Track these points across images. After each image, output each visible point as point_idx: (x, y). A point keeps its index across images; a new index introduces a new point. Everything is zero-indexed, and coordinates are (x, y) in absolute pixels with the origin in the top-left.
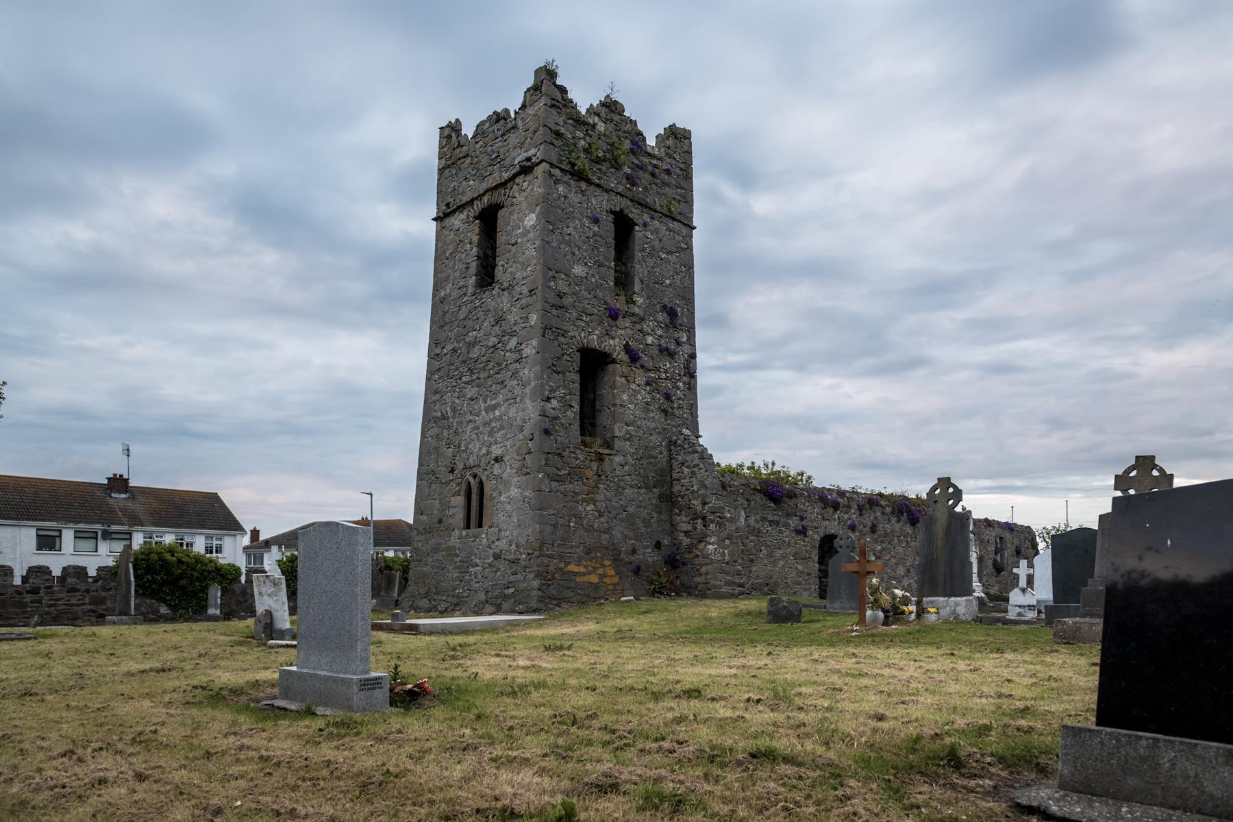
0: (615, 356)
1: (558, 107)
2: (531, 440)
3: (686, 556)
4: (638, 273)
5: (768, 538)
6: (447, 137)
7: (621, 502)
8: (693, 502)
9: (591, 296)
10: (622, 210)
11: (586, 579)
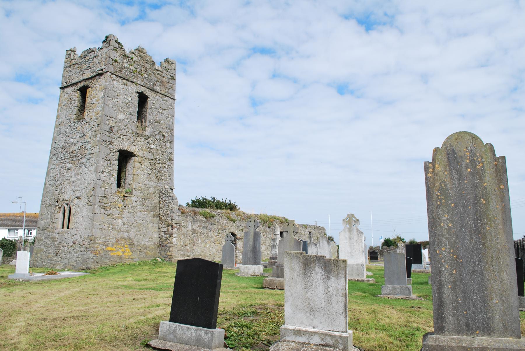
0: (135, 154)
1: (116, 50)
2: (93, 190)
3: (164, 243)
4: (148, 118)
5: (202, 235)
6: (69, 54)
7: (135, 218)
8: (168, 218)
9: (126, 128)
10: (142, 92)
11: (116, 253)
